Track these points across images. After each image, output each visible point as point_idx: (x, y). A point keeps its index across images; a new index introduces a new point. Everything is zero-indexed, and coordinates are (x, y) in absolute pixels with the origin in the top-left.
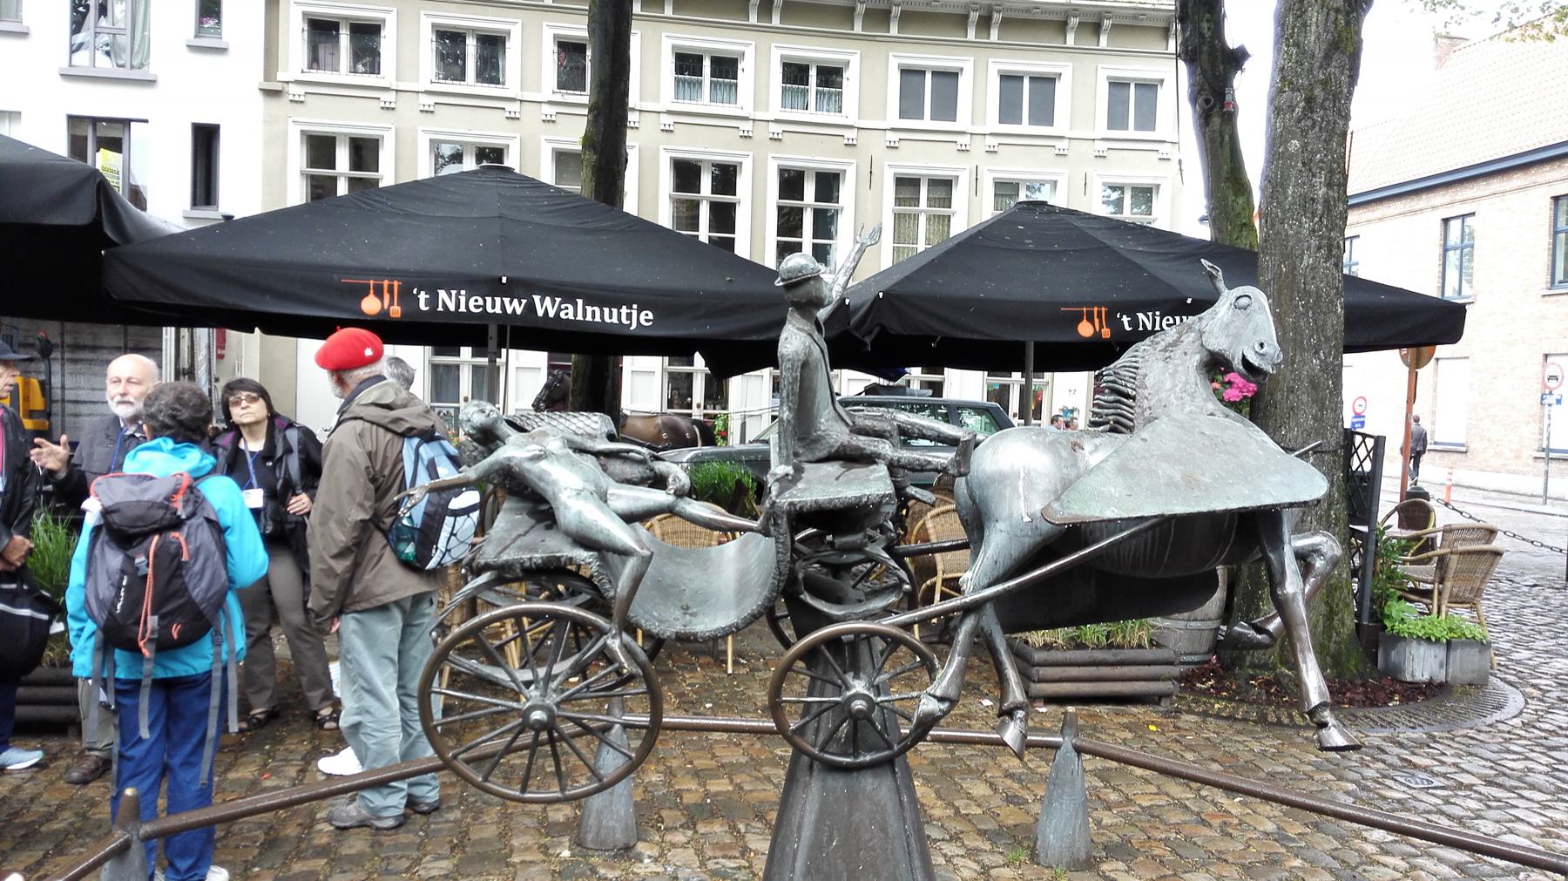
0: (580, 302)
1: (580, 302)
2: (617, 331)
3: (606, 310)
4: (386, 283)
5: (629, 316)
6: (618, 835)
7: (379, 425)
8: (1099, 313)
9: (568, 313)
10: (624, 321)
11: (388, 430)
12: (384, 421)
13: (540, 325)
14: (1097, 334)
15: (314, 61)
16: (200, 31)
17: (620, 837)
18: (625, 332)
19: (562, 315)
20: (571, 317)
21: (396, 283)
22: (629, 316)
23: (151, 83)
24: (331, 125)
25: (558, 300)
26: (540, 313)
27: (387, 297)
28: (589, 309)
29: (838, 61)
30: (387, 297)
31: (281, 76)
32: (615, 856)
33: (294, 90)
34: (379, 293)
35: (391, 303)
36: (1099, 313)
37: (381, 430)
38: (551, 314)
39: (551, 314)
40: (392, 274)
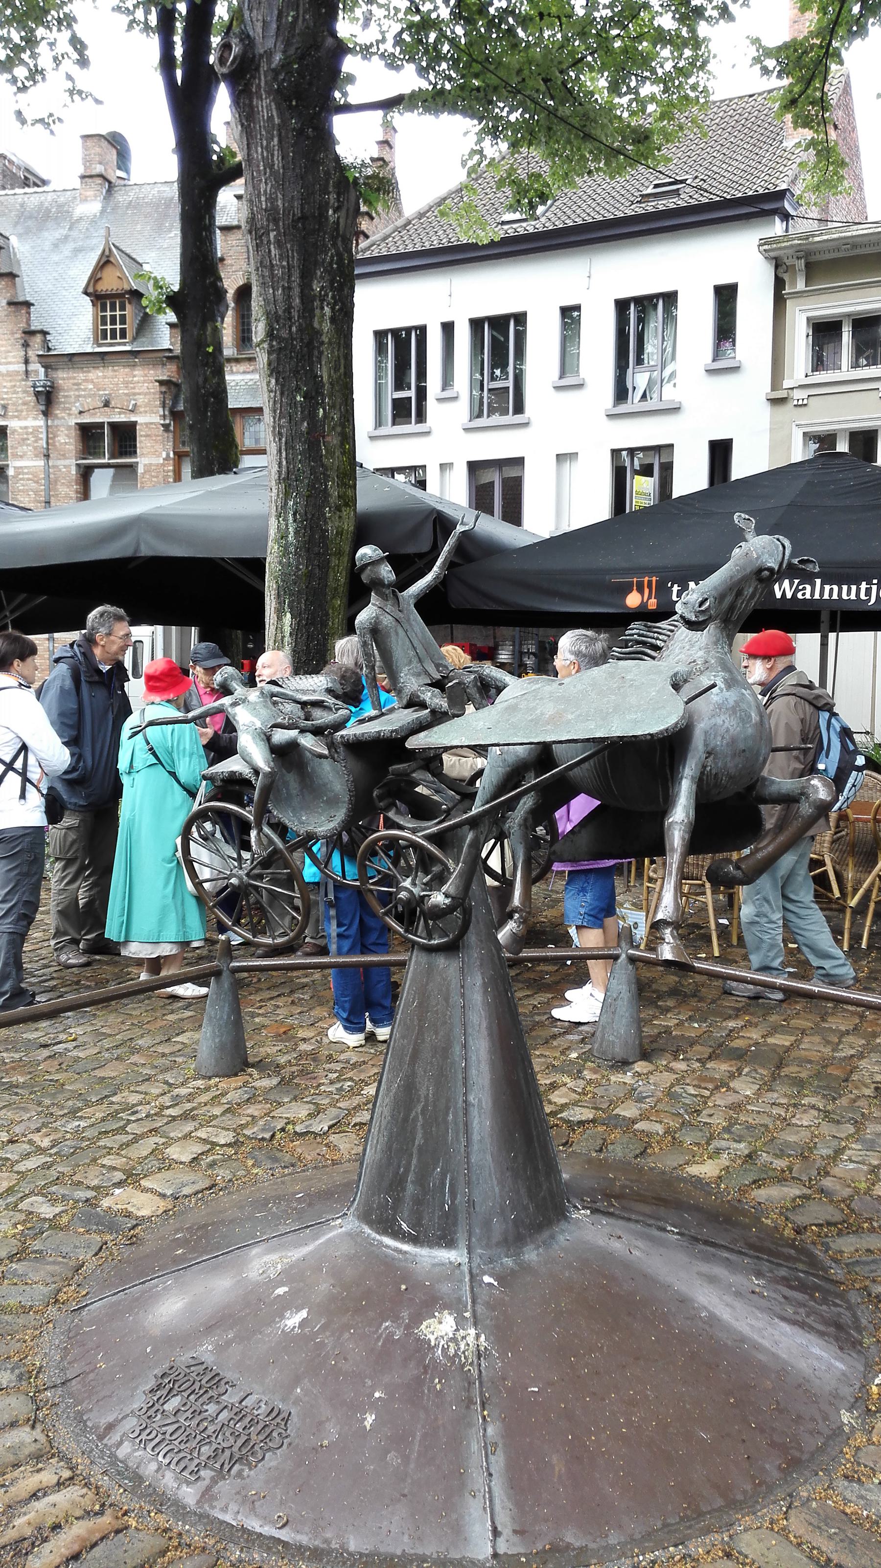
0: (818, 582)
1: (818, 582)
2: (854, 608)
3: (845, 587)
4: (646, 579)
5: (868, 592)
6: (617, 1050)
7: (805, 700)
8: (650, 582)
9: (806, 593)
10: (863, 597)
11: (811, 703)
12: (810, 698)
13: (779, 606)
14: (643, 605)
15: (818, 363)
16: (716, 357)
17: (619, 1051)
18: (862, 608)
19: (800, 596)
20: (808, 596)
21: (654, 579)
22: (868, 592)
23: (675, 410)
24: (854, 421)
25: (796, 581)
26: (778, 595)
27: (646, 591)
28: (827, 588)
29: (833, 316)
30: (646, 591)
31: (787, 384)
32: (612, 1066)
33: (798, 395)
34: (640, 590)
35: (650, 598)
36: (650, 582)
37: (807, 704)
38: (789, 595)
39: (789, 595)
40: (650, 571)
